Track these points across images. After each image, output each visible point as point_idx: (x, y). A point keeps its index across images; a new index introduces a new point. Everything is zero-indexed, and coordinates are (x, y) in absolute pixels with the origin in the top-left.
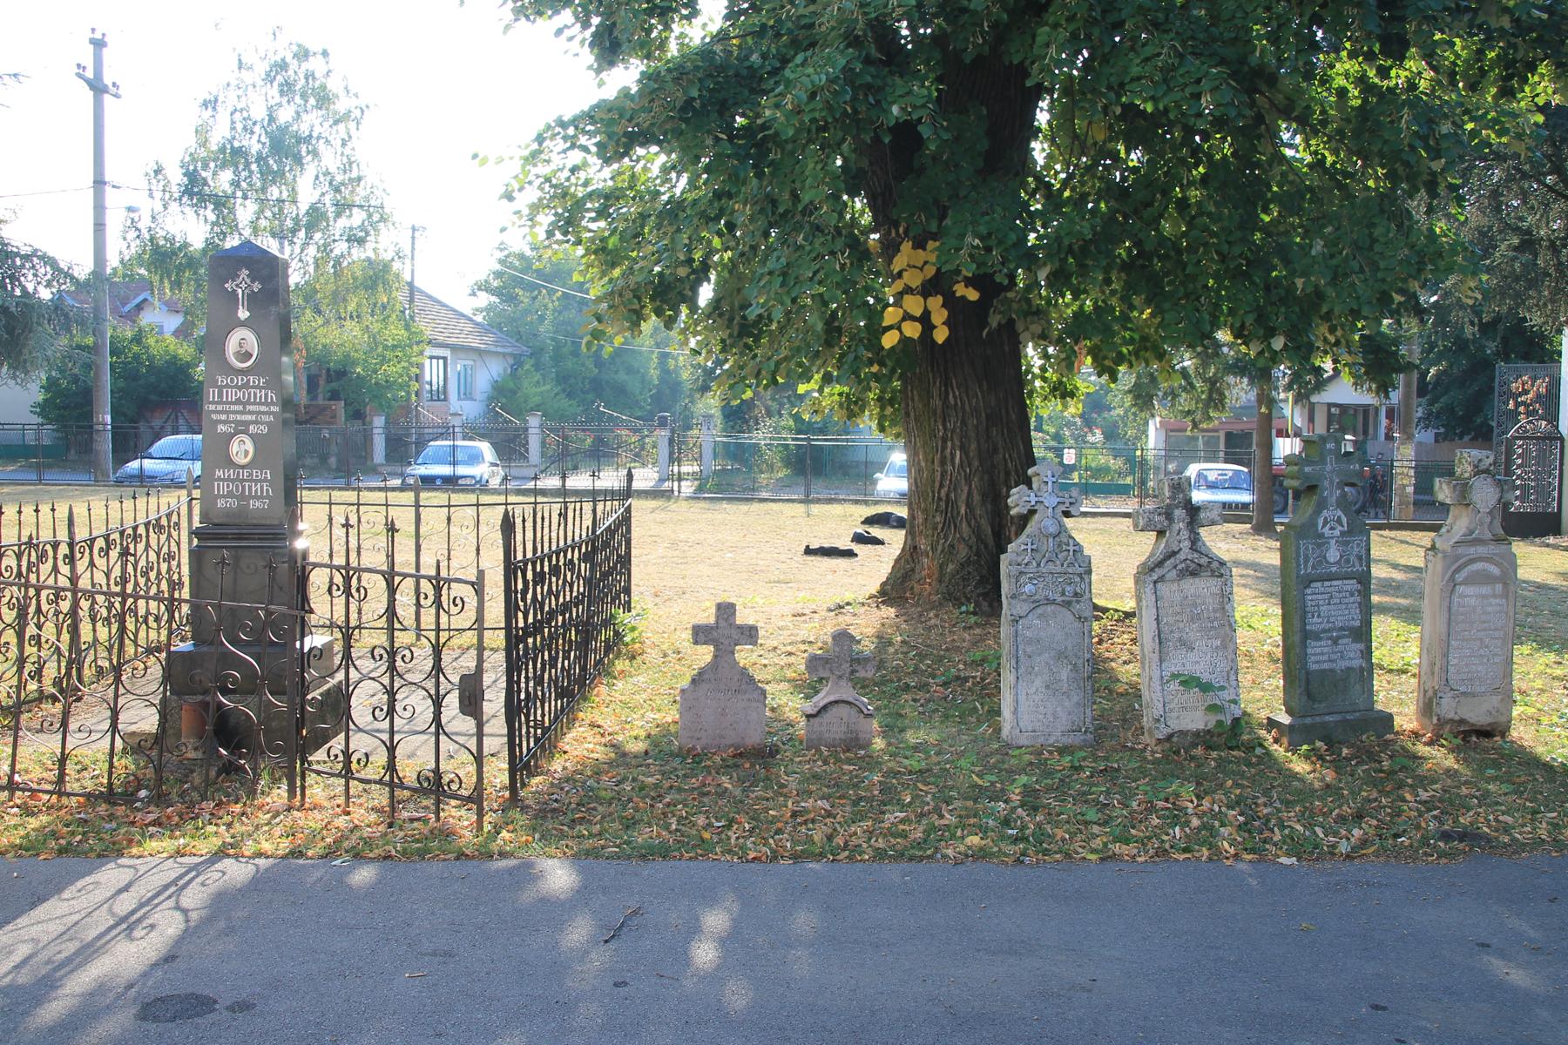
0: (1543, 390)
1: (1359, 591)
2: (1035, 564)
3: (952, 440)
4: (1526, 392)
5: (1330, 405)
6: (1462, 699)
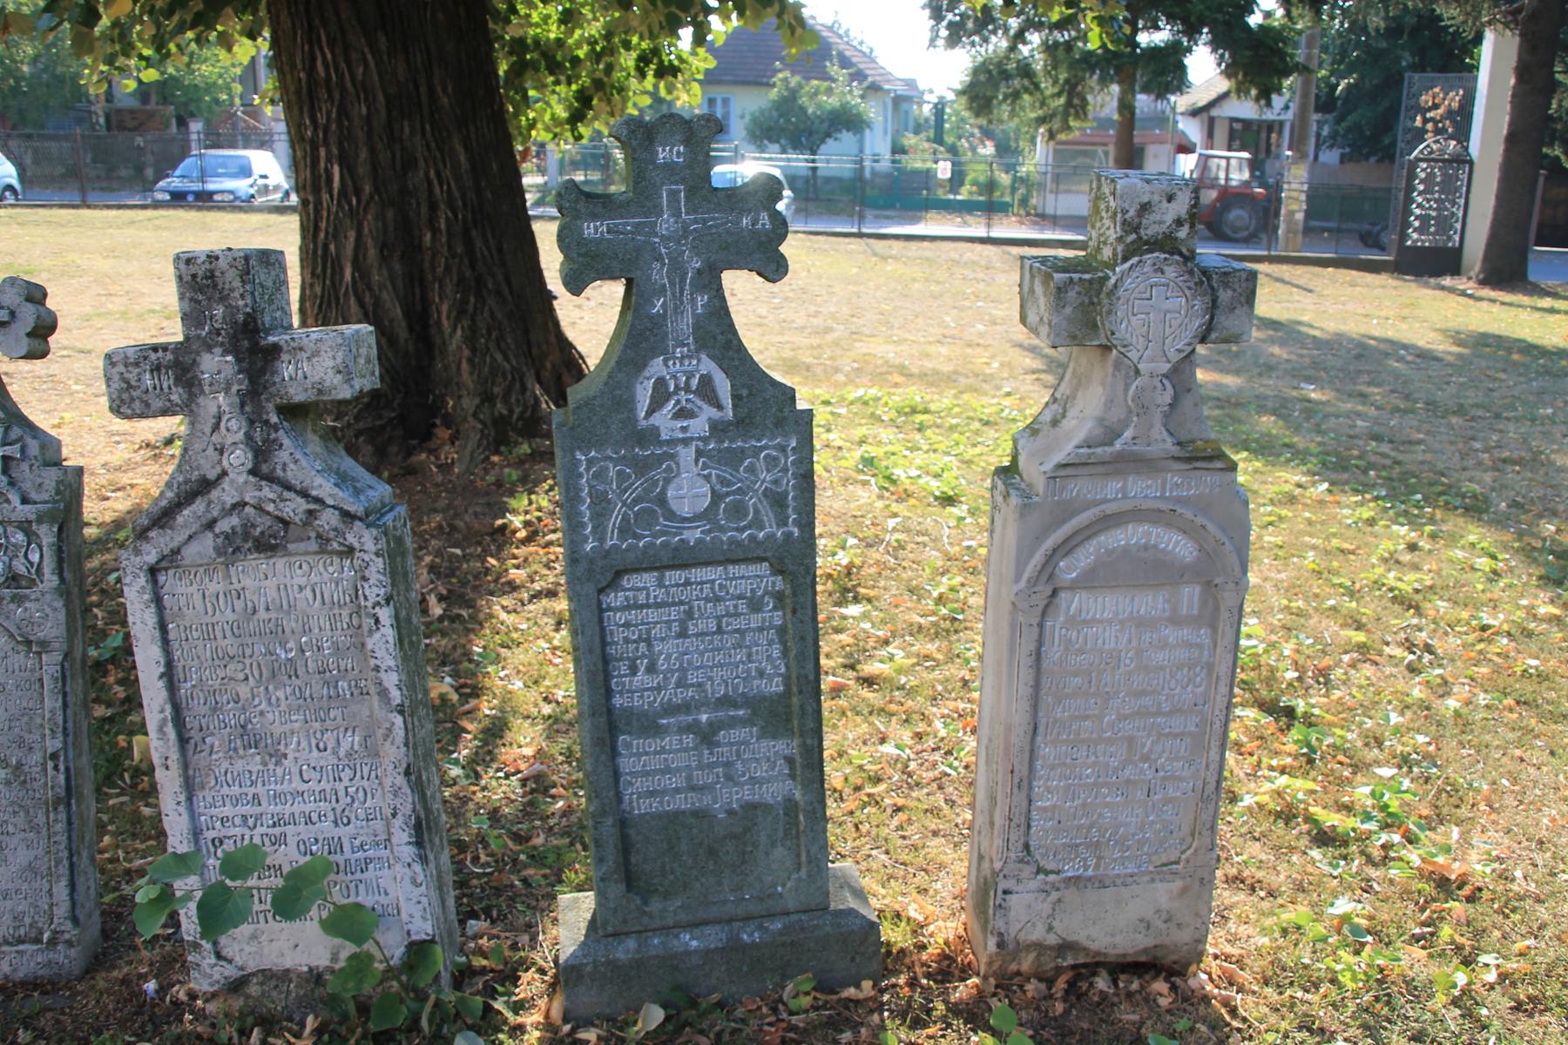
0: (1455, 105)
1: (779, 597)
3: (326, 144)
4: (1436, 107)
5: (1233, 120)
6: (1070, 895)
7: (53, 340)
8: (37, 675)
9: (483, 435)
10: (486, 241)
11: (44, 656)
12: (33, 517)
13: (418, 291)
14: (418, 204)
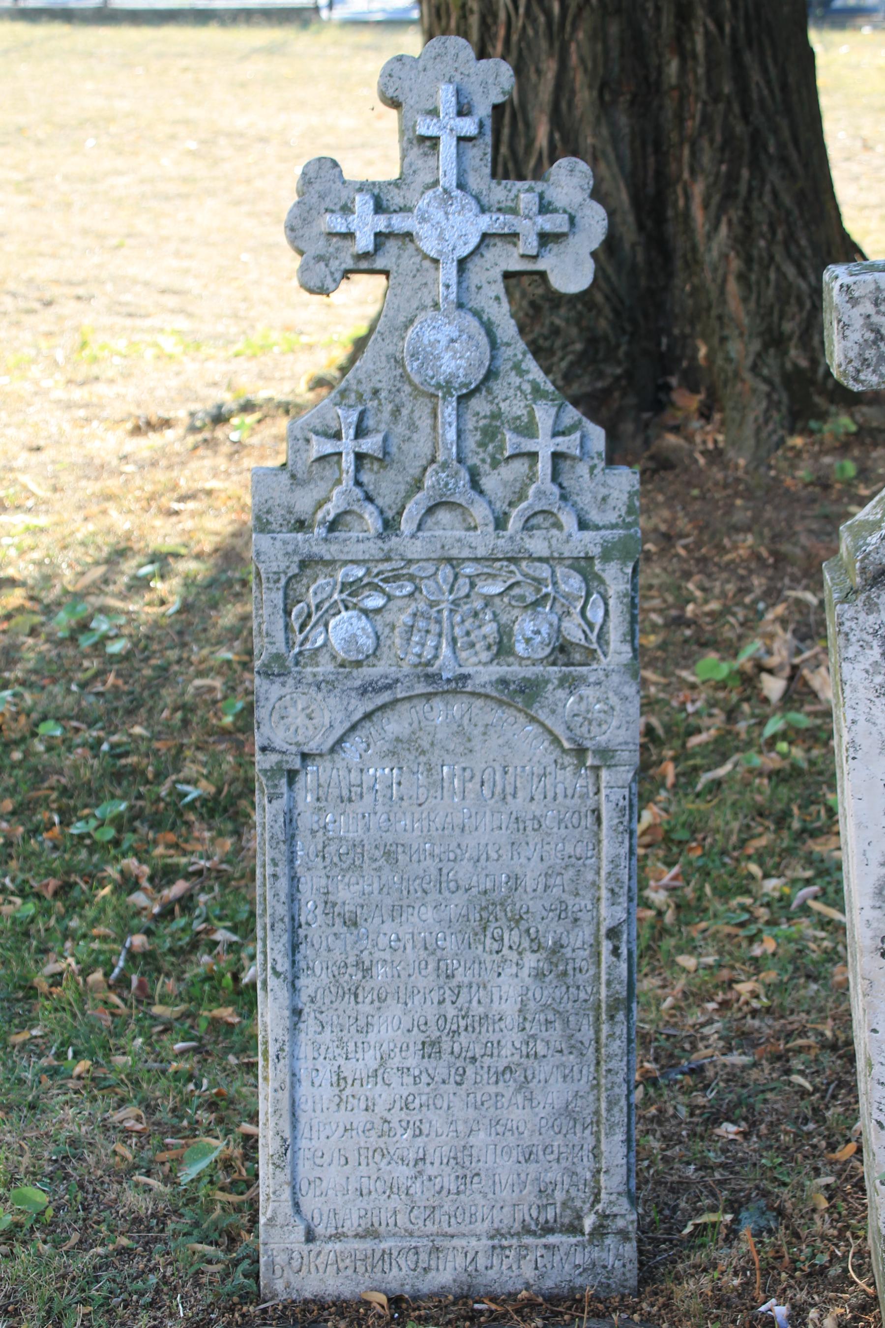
2: (372, 521)
7: (292, 262)
8: (591, 803)
9: (774, 405)
10: (765, 71)
11: (604, 774)
12: (596, 551)
13: (651, 160)
14: (658, 9)
